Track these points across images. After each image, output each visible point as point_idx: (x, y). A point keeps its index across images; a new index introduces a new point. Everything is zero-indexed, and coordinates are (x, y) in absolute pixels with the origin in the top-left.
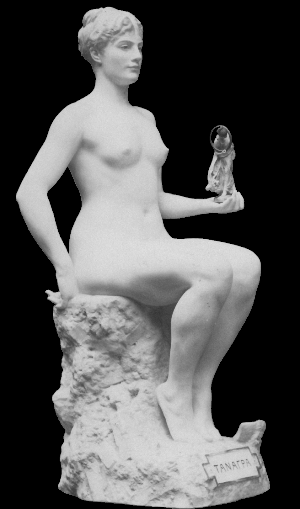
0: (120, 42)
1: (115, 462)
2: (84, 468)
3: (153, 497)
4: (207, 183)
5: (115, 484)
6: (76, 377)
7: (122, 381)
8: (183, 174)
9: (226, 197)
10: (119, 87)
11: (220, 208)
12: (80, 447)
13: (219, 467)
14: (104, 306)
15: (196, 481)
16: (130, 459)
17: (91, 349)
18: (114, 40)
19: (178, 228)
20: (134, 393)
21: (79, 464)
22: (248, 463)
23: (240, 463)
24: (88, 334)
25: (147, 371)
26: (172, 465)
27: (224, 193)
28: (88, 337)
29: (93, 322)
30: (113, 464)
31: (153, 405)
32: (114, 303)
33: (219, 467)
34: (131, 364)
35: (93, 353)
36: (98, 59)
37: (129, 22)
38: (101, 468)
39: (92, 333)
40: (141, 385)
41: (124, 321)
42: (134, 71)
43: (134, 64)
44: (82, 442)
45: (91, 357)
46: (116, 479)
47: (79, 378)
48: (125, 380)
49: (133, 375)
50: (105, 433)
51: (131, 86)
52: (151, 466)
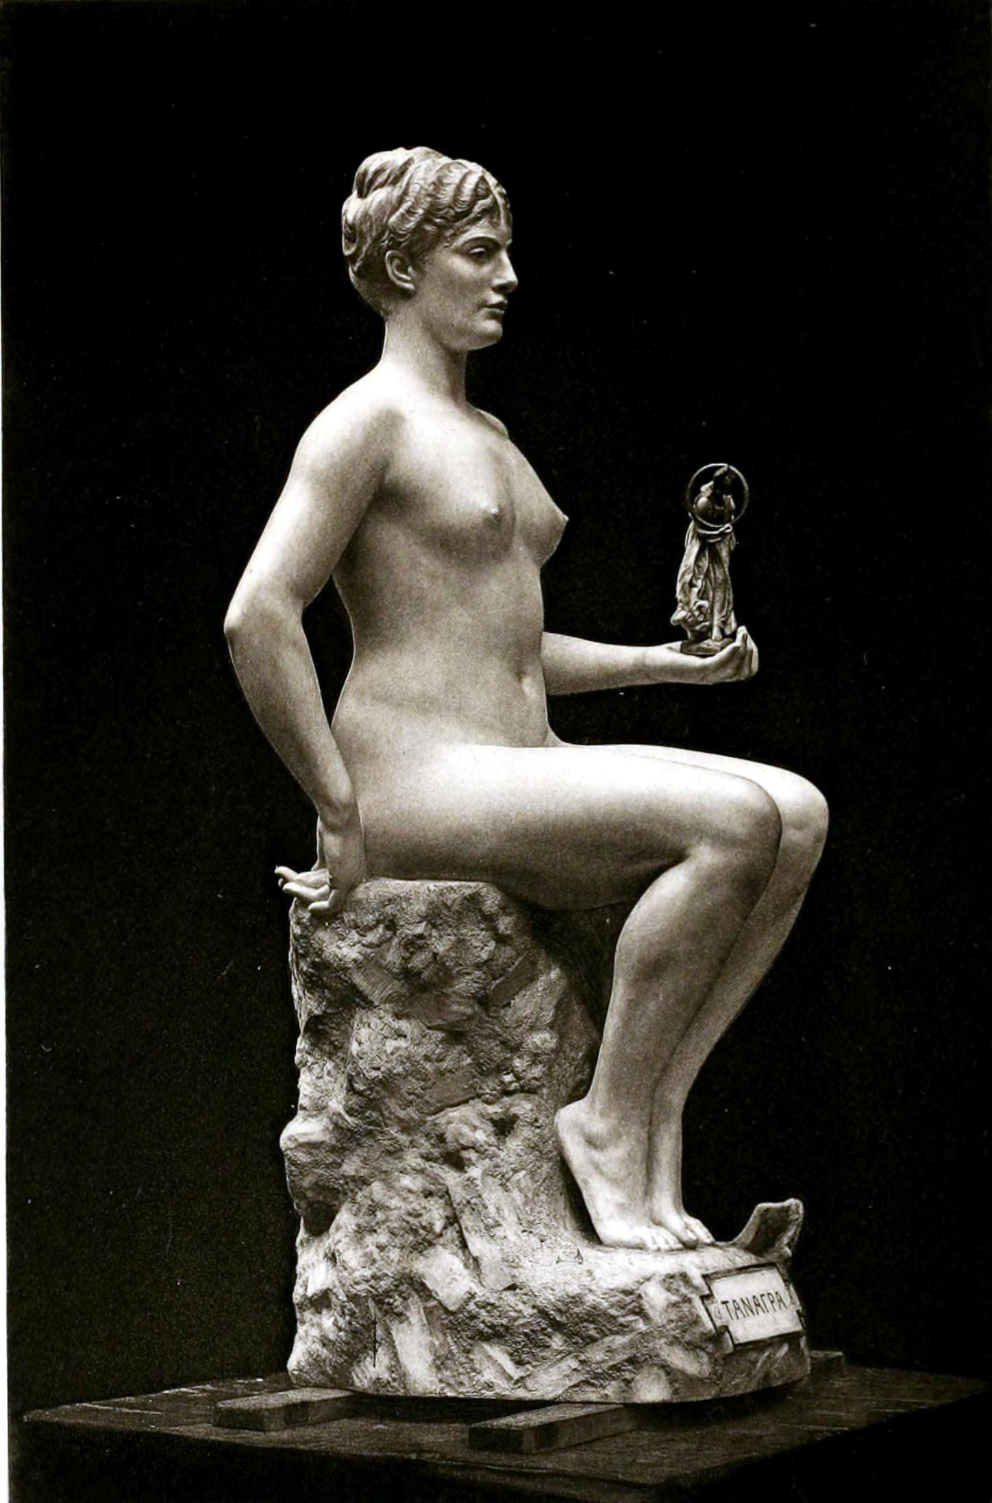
0: (466, 243)
1: (473, 1296)
2: (386, 1313)
3: (576, 1378)
4: (672, 605)
5: (468, 1352)
6: (360, 1086)
7: (473, 1098)
8: (603, 578)
9: (711, 644)
10: (452, 356)
11: (703, 670)
12: (374, 1261)
13: (730, 1305)
14: (448, 908)
15: (687, 1337)
16: (512, 1288)
17: (398, 1016)
18: (455, 236)
19: (585, 715)
20: (504, 1127)
21: (371, 1304)
22: (781, 1300)
23: (766, 1298)
24: (396, 977)
25: (537, 1071)
26: (628, 1299)
27: (716, 632)
28: (396, 986)
29: (414, 944)
30: (467, 1302)
31: (542, 1156)
32: (473, 900)
33: (730, 1305)
34: (498, 1053)
35: (404, 1025)
36: (406, 281)
37: (488, 192)
38: (429, 1312)
39: (408, 974)
40: (523, 1107)
41: (492, 945)
42: (493, 316)
43: (496, 298)
44: (381, 1248)
45: (400, 1035)
46: (472, 1338)
47: (371, 1089)
48: (479, 1096)
49: (502, 1082)
50: (438, 1227)
51: (475, 357)
52: (576, 1300)
